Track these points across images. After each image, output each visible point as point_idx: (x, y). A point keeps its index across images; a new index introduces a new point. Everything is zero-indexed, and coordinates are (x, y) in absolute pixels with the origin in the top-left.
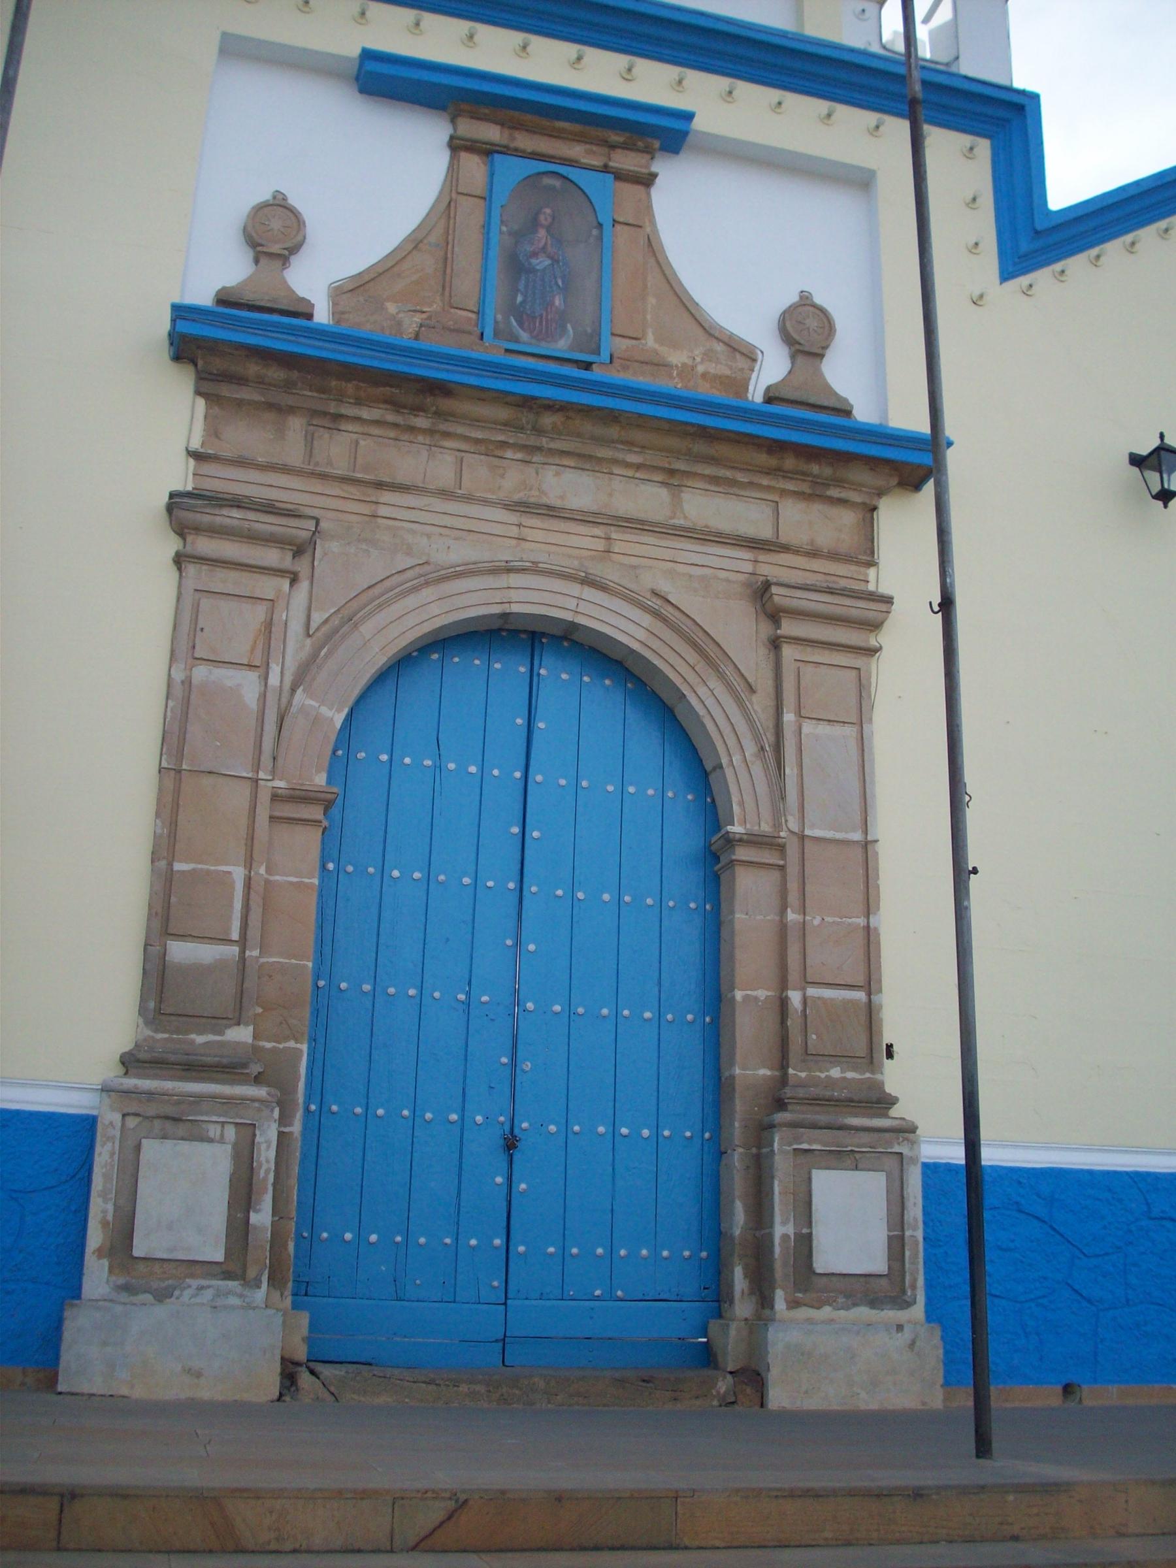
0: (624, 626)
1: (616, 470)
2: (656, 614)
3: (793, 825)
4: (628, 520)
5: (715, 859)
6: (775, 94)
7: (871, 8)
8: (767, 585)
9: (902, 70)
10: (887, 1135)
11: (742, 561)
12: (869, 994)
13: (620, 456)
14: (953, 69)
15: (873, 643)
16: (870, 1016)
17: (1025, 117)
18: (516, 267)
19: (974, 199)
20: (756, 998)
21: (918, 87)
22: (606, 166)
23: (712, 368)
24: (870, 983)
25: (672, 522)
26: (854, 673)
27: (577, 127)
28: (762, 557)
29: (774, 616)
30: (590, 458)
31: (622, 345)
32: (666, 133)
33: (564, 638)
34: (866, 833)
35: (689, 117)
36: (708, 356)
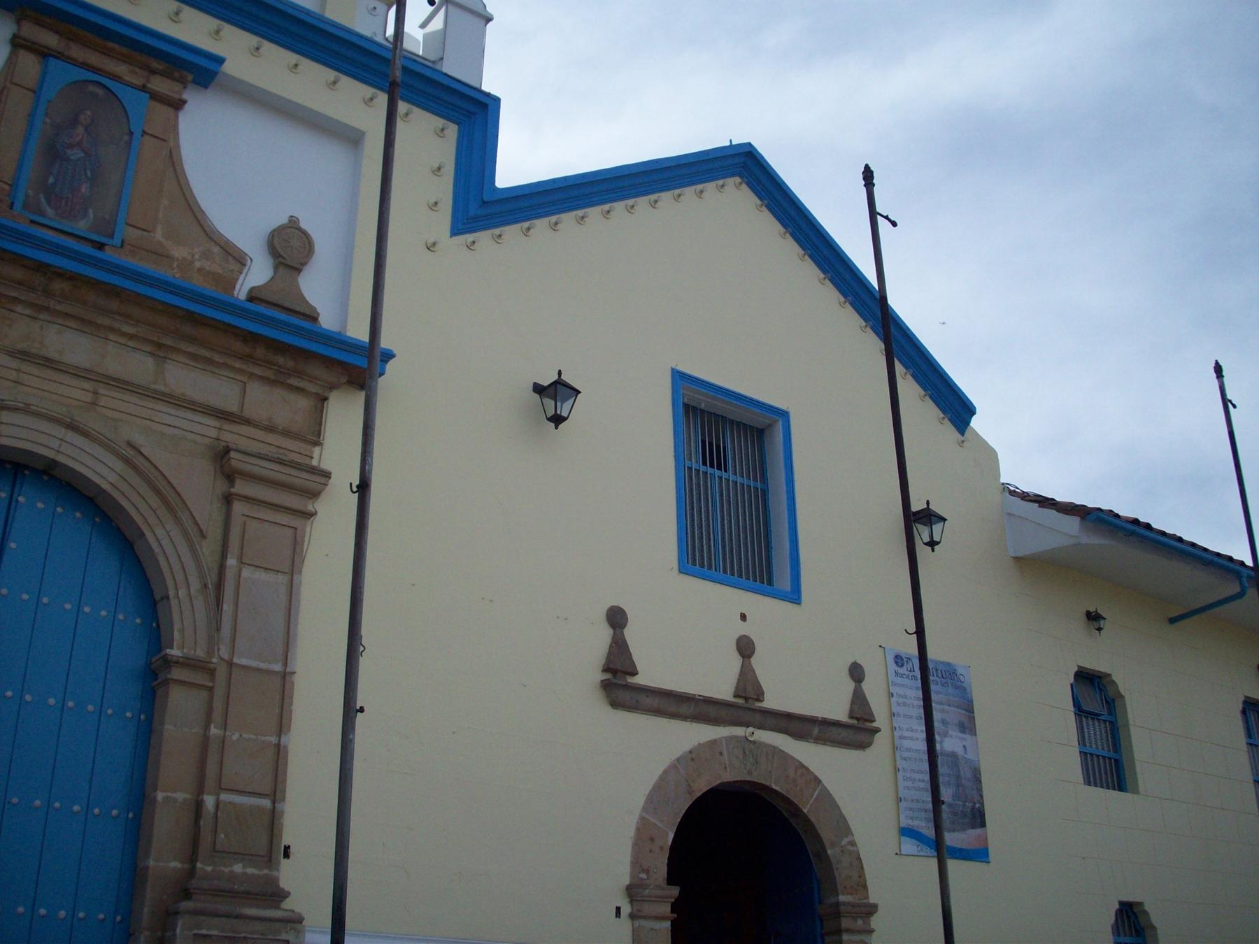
0: (99, 468)
1: (112, 337)
2: (127, 461)
3: (224, 652)
4: (114, 379)
5: (154, 677)
6: (293, 58)
7: (381, 7)
8: (227, 450)
9: (389, 56)
10: (278, 925)
11: (208, 428)
12: (274, 802)
13: (117, 325)
14: (438, 67)
15: (310, 508)
16: (273, 821)
17: (486, 114)
18: (53, 153)
19: (439, 169)
20: (175, 800)
21: (398, 73)
22: (144, 86)
23: (207, 265)
24: (276, 792)
25: (154, 386)
26: (291, 531)
27: (125, 50)
28: (227, 426)
29: (230, 476)
30: (90, 323)
31: (132, 234)
32: (201, 71)
33: (45, 472)
34: (285, 665)
35: (220, 61)
36: (206, 255)
